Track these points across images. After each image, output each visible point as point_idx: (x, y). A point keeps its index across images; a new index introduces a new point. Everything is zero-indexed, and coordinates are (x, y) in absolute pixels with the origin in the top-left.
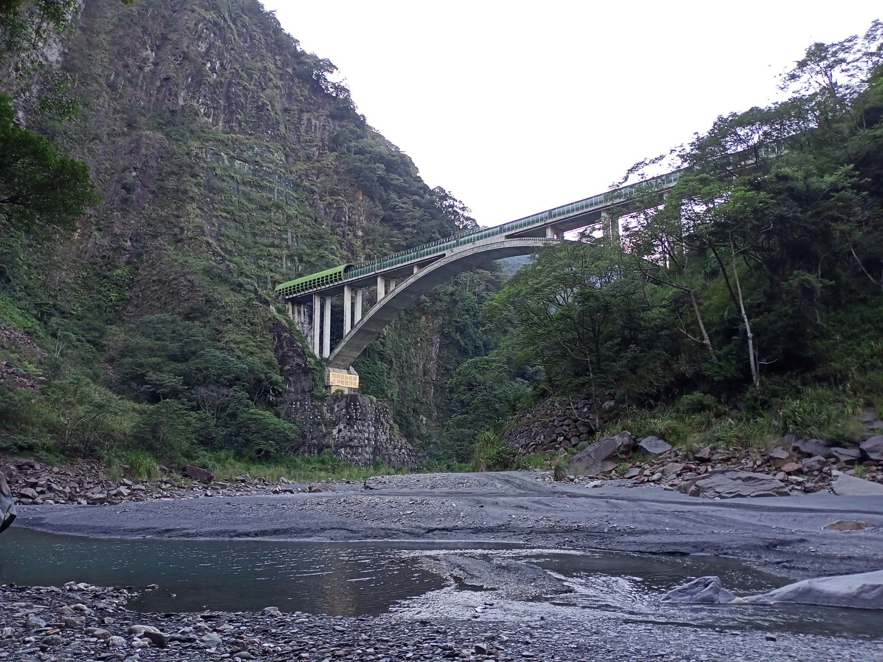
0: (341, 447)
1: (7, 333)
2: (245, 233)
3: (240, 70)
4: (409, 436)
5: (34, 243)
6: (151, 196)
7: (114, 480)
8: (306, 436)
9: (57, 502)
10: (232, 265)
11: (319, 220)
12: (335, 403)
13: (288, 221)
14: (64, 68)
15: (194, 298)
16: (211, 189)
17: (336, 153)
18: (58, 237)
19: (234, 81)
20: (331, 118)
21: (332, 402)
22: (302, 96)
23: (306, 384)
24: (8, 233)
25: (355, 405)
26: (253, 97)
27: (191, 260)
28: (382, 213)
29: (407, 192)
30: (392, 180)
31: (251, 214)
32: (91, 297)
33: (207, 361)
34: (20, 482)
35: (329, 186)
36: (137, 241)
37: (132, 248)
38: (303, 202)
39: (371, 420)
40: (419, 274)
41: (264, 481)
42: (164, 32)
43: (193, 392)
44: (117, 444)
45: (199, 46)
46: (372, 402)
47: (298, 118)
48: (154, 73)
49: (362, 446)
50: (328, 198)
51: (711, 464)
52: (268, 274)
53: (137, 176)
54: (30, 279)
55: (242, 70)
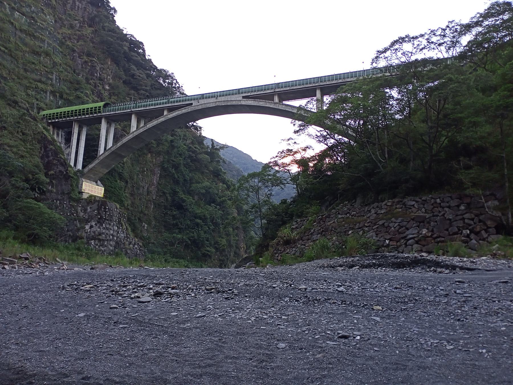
0: (92, 240)
13: (54, 67)
20: (91, 4)
21: (86, 204)
23: (66, 188)
25: (105, 208)
30: (132, 56)
39: (116, 221)
40: (167, 115)
49: (107, 240)
50: (85, 57)
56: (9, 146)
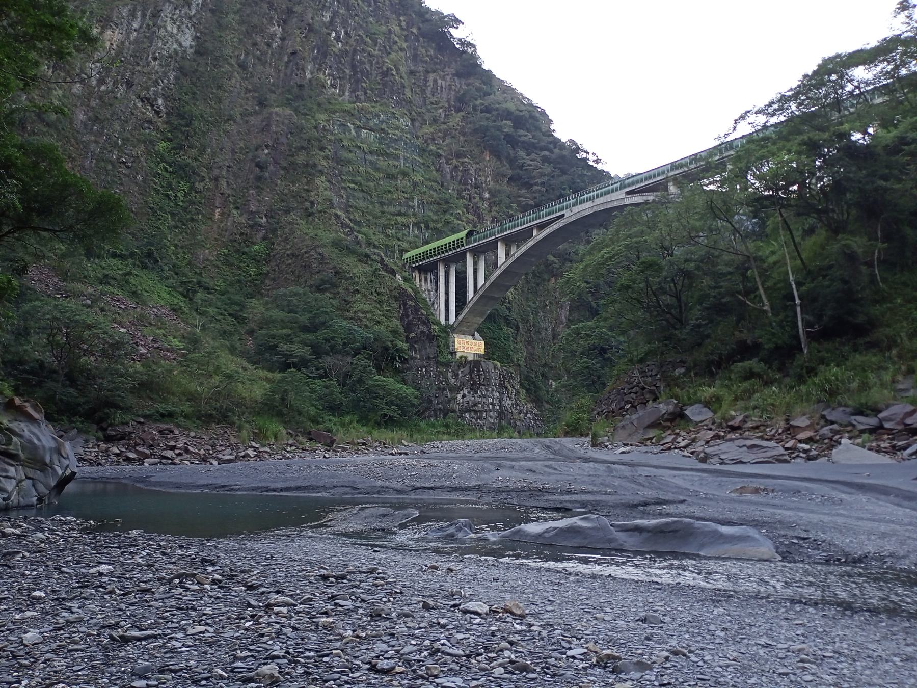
0: (466, 412)
1: (155, 310)
2: (372, 203)
3: (364, 36)
4: (537, 401)
5: (179, 224)
6: (282, 172)
7: (243, 443)
8: (431, 401)
9: (192, 463)
10: (360, 236)
11: (445, 184)
12: (459, 369)
14: (197, 52)
15: (324, 270)
16: (339, 161)
17: (462, 113)
18: (200, 217)
19: (358, 48)
21: (457, 368)
22: (427, 56)
23: (431, 351)
24: (156, 216)
25: (479, 371)
26: (378, 63)
27: (320, 233)
28: (510, 172)
29: (536, 148)
30: (520, 136)
31: (378, 183)
32: (232, 273)
33: (334, 331)
34: (161, 445)
35: (455, 148)
36: (271, 217)
37: (267, 224)
38: (429, 167)
39: (495, 385)
40: (538, 236)
41: (384, 444)
42: (290, 6)
43: (320, 361)
44: (249, 410)
45: (323, 16)
46: (495, 368)
47: (424, 80)
48: (282, 48)
50: (454, 161)
51: (740, 431)
52: (396, 243)
53: (269, 153)
54: (178, 258)
55: (367, 36)
56: (365, 313)
